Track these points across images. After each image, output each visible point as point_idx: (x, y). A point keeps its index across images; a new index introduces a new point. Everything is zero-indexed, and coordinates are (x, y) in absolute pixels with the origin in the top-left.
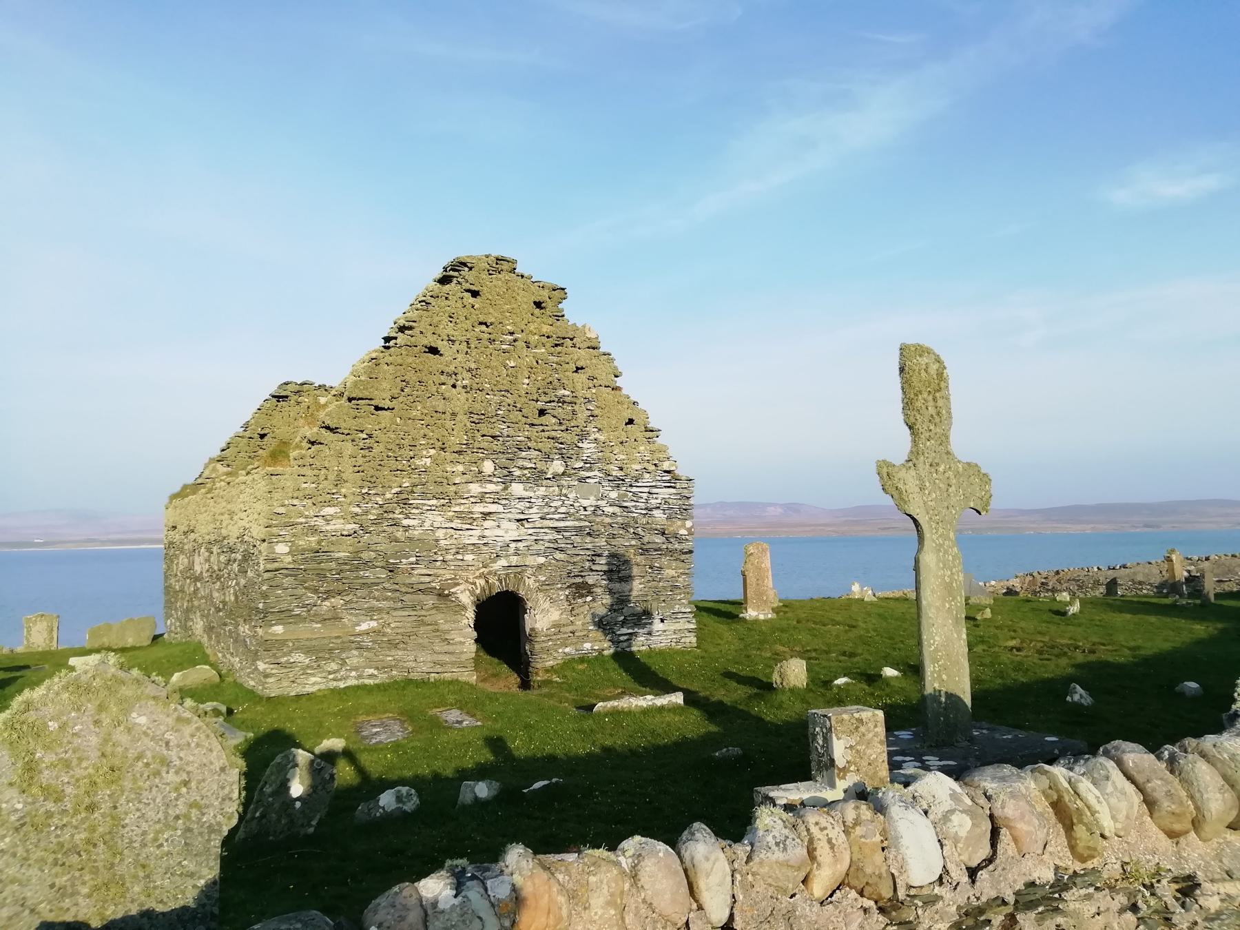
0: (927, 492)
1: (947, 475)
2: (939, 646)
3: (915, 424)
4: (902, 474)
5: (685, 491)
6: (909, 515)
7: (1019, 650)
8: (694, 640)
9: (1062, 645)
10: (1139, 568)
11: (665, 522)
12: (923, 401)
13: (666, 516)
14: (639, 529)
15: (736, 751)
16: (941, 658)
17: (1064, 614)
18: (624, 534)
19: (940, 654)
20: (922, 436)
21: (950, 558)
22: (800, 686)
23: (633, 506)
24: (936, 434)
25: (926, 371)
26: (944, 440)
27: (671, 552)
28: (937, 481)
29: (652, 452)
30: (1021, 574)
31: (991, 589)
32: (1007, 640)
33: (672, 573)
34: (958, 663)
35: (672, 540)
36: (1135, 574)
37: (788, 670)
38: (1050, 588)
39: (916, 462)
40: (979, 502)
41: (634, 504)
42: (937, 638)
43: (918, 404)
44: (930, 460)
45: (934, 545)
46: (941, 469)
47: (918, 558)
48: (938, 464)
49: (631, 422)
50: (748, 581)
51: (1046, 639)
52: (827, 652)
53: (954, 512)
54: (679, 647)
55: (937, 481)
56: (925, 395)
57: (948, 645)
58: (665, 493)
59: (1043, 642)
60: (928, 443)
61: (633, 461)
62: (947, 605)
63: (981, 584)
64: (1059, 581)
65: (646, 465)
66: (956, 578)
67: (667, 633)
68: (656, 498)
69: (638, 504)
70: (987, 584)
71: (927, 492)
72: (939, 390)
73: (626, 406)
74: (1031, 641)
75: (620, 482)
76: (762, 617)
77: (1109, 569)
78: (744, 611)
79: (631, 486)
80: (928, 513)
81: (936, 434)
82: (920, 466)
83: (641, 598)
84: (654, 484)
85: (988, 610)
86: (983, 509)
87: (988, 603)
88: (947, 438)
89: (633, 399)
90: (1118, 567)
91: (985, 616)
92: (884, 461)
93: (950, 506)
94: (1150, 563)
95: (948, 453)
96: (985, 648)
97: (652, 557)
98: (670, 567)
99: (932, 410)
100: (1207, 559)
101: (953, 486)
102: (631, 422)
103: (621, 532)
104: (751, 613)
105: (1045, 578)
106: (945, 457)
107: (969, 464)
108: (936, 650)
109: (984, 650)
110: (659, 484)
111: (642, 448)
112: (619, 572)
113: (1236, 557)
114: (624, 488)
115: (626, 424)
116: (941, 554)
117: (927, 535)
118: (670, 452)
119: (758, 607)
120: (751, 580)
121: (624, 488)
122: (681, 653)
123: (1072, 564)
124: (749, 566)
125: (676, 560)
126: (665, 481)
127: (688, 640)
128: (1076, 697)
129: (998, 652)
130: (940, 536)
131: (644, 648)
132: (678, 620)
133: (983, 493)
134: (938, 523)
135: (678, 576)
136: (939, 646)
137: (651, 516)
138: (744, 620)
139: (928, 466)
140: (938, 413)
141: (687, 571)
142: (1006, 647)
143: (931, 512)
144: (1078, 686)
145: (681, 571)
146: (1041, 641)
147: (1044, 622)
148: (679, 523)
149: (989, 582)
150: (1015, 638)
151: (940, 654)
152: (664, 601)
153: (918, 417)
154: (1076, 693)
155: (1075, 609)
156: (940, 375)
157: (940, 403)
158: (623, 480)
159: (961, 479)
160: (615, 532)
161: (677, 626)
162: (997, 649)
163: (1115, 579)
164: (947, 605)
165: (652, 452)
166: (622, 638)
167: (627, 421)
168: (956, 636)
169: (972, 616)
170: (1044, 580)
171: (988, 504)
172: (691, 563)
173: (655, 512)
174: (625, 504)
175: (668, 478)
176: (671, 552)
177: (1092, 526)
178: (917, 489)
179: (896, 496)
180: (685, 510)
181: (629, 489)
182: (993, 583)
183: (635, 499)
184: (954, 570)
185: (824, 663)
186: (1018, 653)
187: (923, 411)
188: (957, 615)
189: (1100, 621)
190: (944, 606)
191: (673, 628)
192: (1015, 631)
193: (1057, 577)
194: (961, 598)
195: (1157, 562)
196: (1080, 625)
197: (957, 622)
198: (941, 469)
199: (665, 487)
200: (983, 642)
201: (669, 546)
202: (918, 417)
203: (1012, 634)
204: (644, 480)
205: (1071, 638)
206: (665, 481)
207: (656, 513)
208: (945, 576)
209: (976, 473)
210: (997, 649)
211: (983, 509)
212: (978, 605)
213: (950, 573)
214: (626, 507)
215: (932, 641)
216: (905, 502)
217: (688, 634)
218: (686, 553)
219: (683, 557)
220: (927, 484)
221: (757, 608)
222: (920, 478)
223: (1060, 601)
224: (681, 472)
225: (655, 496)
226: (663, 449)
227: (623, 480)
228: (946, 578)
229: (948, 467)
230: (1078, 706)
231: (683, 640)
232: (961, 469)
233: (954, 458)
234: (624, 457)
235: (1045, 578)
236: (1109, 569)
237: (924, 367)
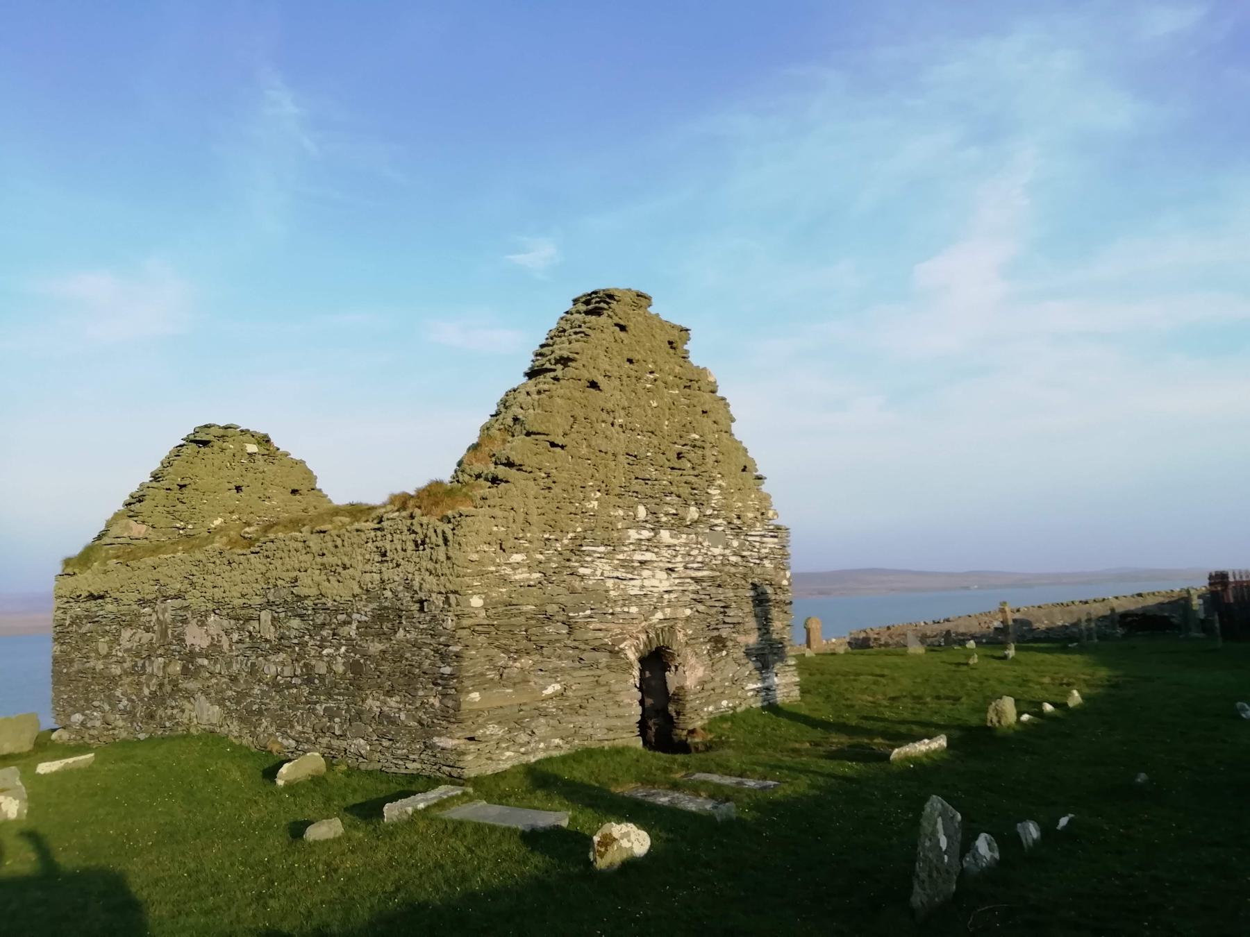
15: (940, 820)
38: (883, 642)
64: (890, 636)
100: (1018, 611)
105: (878, 634)
170: (876, 636)
182: (834, 640)
235: (878, 634)
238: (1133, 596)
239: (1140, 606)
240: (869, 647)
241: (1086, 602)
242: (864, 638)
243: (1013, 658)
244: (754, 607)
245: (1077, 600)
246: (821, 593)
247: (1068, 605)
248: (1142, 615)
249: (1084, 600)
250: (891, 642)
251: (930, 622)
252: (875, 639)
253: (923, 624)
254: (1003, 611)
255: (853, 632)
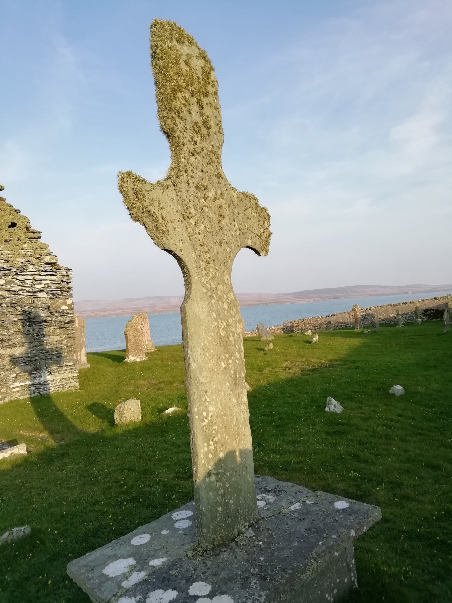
0: (192, 221)
1: (218, 203)
2: (214, 417)
3: (174, 130)
4: (157, 193)
5: (65, 278)
6: (170, 252)
7: (290, 369)
8: (77, 384)
9: (314, 363)
10: (340, 316)
11: (49, 301)
12: (183, 102)
13: (49, 296)
14: (26, 307)
15: (25, 529)
16: (217, 433)
17: (310, 342)
18: (12, 311)
19: (216, 427)
20: (185, 148)
21: (226, 305)
22: (136, 420)
23: (20, 290)
24: (203, 149)
25: (187, 63)
26: (214, 159)
27: (56, 323)
28: (206, 209)
29: (34, 249)
30: (286, 322)
31: (272, 331)
32: (283, 362)
33: (57, 338)
34: (239, 434)
35: (55, 314)
36: (338, 318)
37: (125, 409)
38: (300, 328)
39: (177, 180)
40: (257, 240)
41: (20, 288)
42: (211, 408)
43: (177, 104)
44: (196, 181)
45: (204, 290)
46: (211, 194)
47: (184, 308)
48: (206, 188)
49: (13, 225)
50: (129, 338)
51: (304, 360)
52: (172, 383)
53: (229, 250)
54: (65, 390)
55: (206, 209)
56: (187, 95)
57: (225, 415)
58: (47, 279)
59: (303, 362)
60: (193, 159)
61: (18, 255)
62: (223, 365)
63: (268, 329)
64: (304, 324)
65: (30, 259)
66: (233, 329)
67: (55, 382)
68: (40, 284)
69: (24, 288)
70: (271, 329)
71: (192, 221)
72: (206, 95)
73: (8, 213)
74: (296, 362)
75: (7, 272)
76: (138, 360)
77: (327, 317)
78: (126, 357)
79: (17, 274)
80: (195, 249)
81: (203, 149)
82: (183, 187)
83: (30, 359)
84: (37, 273)
85: (271, 344)
86: (263, 249)
87: (271, 339)
88: (218, 157)
89: (15, 207)
90: (330, 316)
91: (270, 348)
92: (129, 173)
93: (223, 242)
94: (345, 313)
95: (219, 176)
96: (270, 369)
97: (39, 327)
98: (54, 334)
99: (196, 117)
100: (370, 309)
101: (227, 218)
102: (13, 225)
103: (9, 310)
104: (131, 358)
105: (297, 323)
106: (216, 180)
107: (245, 194)
108: (211, 423)
109: (270, 371)
110: (42, 272)
111: (25, 246)
112: (9, 340)
113: (382, 307)
114: (11, 277)
115: (10, 227)
116: (213, 301)
117: (195, 278)
118: (51, 249)
119: (136, 354)
120: (131, 336)
121: (11, 277)
122: (67, 394)
123: (308, 316)
124: (129, 328)
125: (60, 328)
126: (47, 271)
127: (72, 385)
128: (332, 408)
129: (278, 372)
130: (212, 279)
131: (35, 395)
132: (63, 372)
133: (262, 230)
134: (208, 263)
135: (63, 340)
136: (214, 417)
137: (36, 297)
138: (127, 363)
139: (193, 188)
140: (205, 123)
141: (69, 336)
142: (282, 367)
143: (199, 248)
144: (332, 399)
145: (65, 336)
146: (301, 362)
147: (301, 348)
148: (61, 301)
149: (272, 327)
150: (287, 361)
151: (216, 427)
152: (51, 359)
153: (178, 121)
154: (331, 404)
155: (315, 339)
156: (207, 74)
157: (207, 111)
158: (10, 270)
159: (236, 211)
160: (4, 311)
161: (63, 376)
162: (277, 370)
163: (330, 321)
164: (223, 365)
165: (34, 249)
166: (15, 390)
167: (10, 224)
168: (235, 401)
169: (263, 348)
170: (297, 325)
171: (267, 243)
172: (73, 330)
173: (40, 294)
174: (13, 289)
175: (50, 268)
176: (56, 323)
177: (313, 299)
178: (178, 217)
179: (150, 225)
180: (67, 291)
181: (15, 277)
182: (273, 327)
183: (21, 284)
184: (230, 321)
185: (167, 392)
186: (289, 371)
187: (185, 114)
188: (235, 374)
189: (329, 345)
190: (220, 366)
191: (59, 378)
192: (286, 356)
193: (303, 323)
194: (240, 353)
195: (348, 312)
196: (319, 348)
197: (236, 384)
198: (211, 194)
199: (48, 275)
200: (269, 365)
201: (53, 319)
202: (178, 121)
203: (285, 358)
204: (28, 270)
205: (318, 358)
206: (47, 271)
207: (41, 294)
208: (219, 328)
209: (253, 206)
210: (277, 370)
211: (263, 249)
212: (266, 341)
213: (225, 324)
214: (14, 291)
215: (205, 414)
216: (163, 233)
217: (72, 381)
218: (68, 323)
219: (65, 326)
220: (193, 212)
221: (135, 354)
222: (183, 203)
223: (307, 335)
224: (62, 263)
225: (38, 282)
226: (45, 247)
227: (10, 270)
228: (221, 331)
229: (219, 193)
230: (334, 414)
231: (68, 386)
232: (235, 199)
233: (227, 184)
234: (9, 252)
235: (297, 323)
236: (327, 317)
237: (184, 58)
238: (431, 299)
239: (435, 305)
240: (293, 331)
241: (406, 304)
242: (290, 326)
243: (315, 342)
244: (23, 327)
245: (401, 302)
246: (335, 298)
247: (396, 305)
248: (436, 310)
249: (405, 302)
250: (304, 328)
251: (324, 316)
252: (296, 326)
253: (321, 317)
254: (354, 310)
255: (285, 322)
